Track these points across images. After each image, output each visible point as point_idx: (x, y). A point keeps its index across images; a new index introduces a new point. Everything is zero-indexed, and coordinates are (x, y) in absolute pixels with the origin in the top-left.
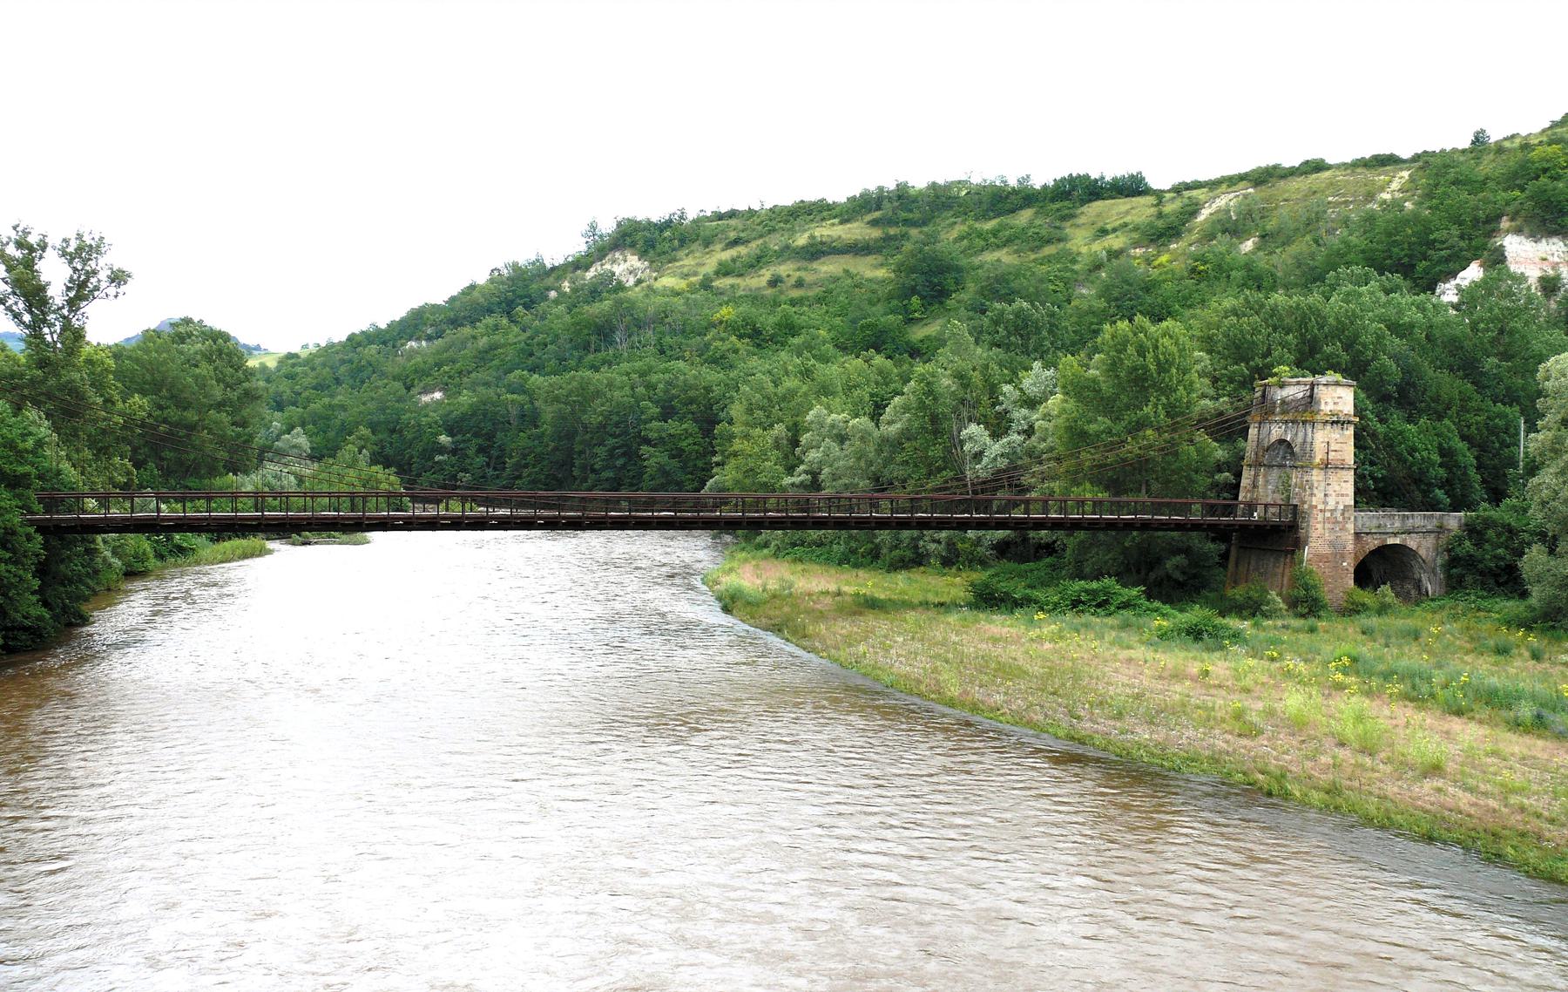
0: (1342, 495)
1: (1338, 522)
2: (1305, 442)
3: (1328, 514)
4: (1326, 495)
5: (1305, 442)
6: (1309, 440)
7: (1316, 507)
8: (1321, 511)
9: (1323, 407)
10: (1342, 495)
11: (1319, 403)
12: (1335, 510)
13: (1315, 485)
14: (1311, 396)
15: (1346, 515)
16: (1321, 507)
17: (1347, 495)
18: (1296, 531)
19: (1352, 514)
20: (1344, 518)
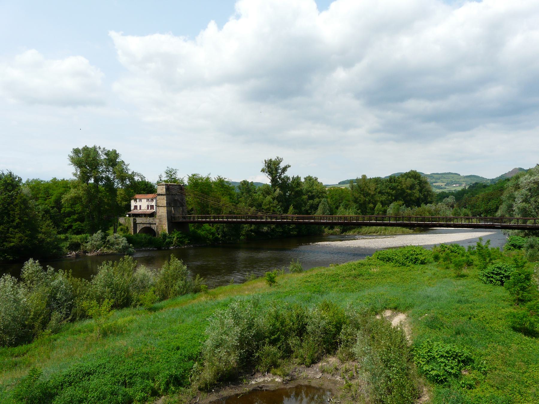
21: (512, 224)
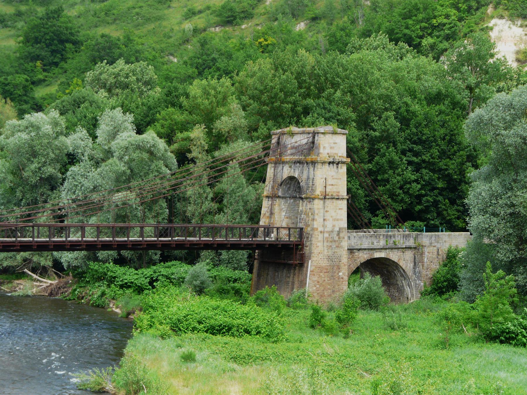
0: (338, 220)
1: (335, 241)
2: (308, 178)
3: (326, 235)
4: (324, 220)
5: (308, 178)
6: (311, 176)
7: (317, 229)
8: (321, 232)
9: (321, 150)
10: (338, 220)
11: (318, 148)
12: (332, 231)
13: (316, 212)
14: (313, 142)
15: (342, 235)
16: (321, 229)
17: (342, 220)
18: (302, 249)
19: (345, 234)
20: (339, 238)
21: (74, 237)
